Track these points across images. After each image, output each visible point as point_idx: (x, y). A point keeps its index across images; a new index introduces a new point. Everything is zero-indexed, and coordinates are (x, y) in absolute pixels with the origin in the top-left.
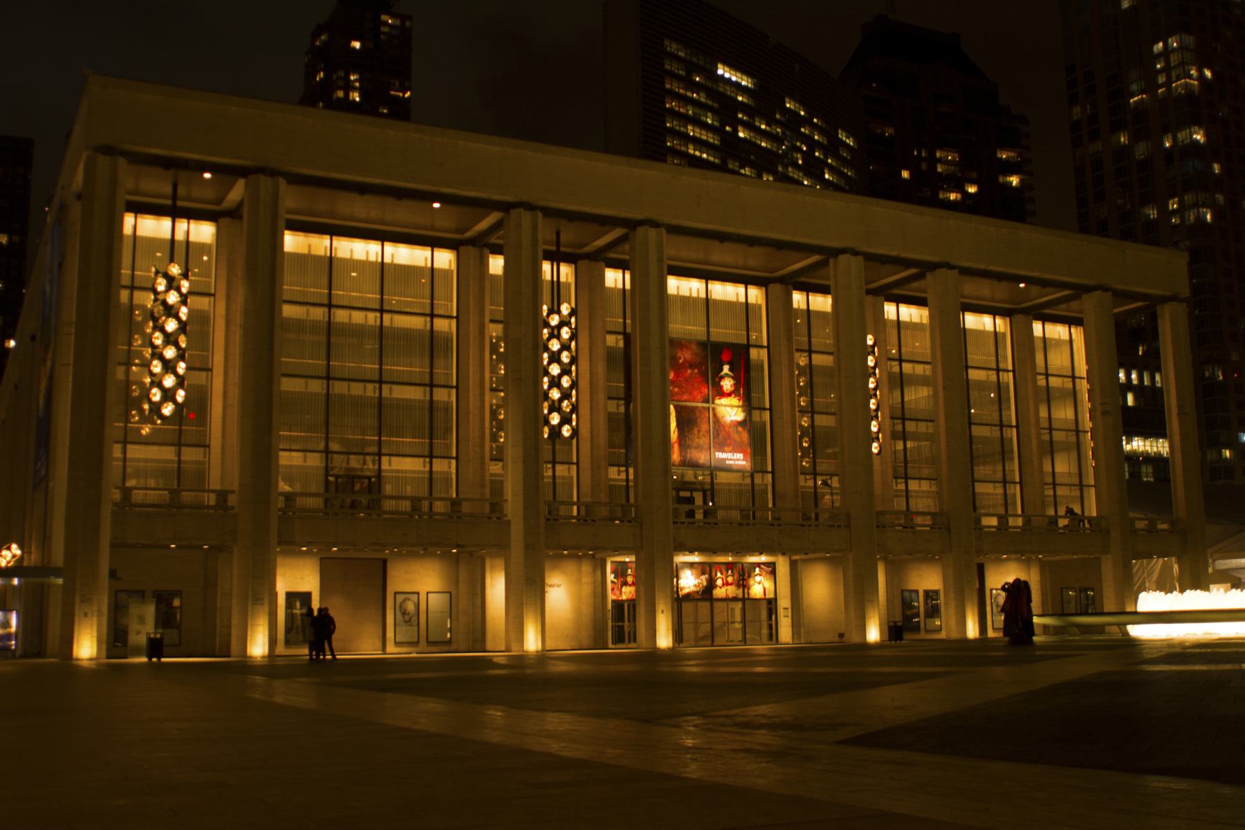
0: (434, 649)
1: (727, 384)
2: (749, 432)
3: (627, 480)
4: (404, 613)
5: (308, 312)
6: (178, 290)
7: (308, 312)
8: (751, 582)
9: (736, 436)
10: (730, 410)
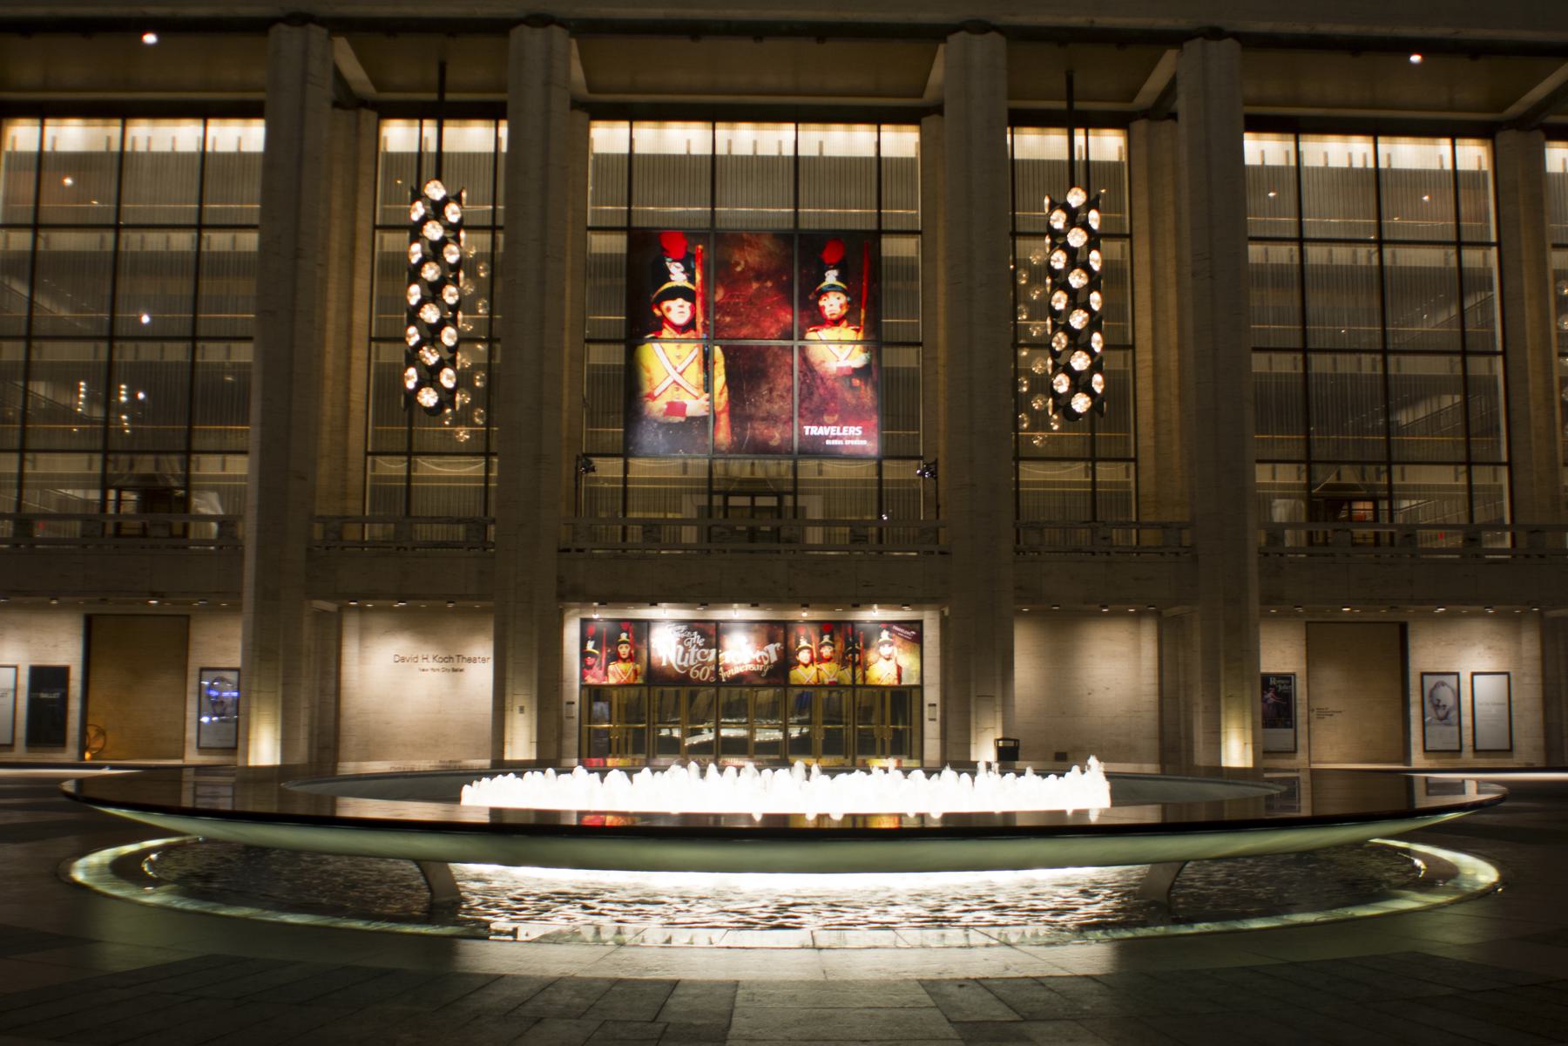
0: (1483, 762)
1: (833, 304)
2: (875, 386)
3: (487, 479)
4: (1437, 706)
5: (234, 240)
6: (1086, 226)
7: (234, 240)
8: (872, 656)
9: (848, 396)
10: (837, 350)
